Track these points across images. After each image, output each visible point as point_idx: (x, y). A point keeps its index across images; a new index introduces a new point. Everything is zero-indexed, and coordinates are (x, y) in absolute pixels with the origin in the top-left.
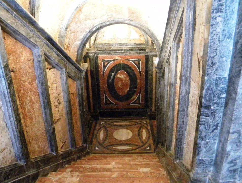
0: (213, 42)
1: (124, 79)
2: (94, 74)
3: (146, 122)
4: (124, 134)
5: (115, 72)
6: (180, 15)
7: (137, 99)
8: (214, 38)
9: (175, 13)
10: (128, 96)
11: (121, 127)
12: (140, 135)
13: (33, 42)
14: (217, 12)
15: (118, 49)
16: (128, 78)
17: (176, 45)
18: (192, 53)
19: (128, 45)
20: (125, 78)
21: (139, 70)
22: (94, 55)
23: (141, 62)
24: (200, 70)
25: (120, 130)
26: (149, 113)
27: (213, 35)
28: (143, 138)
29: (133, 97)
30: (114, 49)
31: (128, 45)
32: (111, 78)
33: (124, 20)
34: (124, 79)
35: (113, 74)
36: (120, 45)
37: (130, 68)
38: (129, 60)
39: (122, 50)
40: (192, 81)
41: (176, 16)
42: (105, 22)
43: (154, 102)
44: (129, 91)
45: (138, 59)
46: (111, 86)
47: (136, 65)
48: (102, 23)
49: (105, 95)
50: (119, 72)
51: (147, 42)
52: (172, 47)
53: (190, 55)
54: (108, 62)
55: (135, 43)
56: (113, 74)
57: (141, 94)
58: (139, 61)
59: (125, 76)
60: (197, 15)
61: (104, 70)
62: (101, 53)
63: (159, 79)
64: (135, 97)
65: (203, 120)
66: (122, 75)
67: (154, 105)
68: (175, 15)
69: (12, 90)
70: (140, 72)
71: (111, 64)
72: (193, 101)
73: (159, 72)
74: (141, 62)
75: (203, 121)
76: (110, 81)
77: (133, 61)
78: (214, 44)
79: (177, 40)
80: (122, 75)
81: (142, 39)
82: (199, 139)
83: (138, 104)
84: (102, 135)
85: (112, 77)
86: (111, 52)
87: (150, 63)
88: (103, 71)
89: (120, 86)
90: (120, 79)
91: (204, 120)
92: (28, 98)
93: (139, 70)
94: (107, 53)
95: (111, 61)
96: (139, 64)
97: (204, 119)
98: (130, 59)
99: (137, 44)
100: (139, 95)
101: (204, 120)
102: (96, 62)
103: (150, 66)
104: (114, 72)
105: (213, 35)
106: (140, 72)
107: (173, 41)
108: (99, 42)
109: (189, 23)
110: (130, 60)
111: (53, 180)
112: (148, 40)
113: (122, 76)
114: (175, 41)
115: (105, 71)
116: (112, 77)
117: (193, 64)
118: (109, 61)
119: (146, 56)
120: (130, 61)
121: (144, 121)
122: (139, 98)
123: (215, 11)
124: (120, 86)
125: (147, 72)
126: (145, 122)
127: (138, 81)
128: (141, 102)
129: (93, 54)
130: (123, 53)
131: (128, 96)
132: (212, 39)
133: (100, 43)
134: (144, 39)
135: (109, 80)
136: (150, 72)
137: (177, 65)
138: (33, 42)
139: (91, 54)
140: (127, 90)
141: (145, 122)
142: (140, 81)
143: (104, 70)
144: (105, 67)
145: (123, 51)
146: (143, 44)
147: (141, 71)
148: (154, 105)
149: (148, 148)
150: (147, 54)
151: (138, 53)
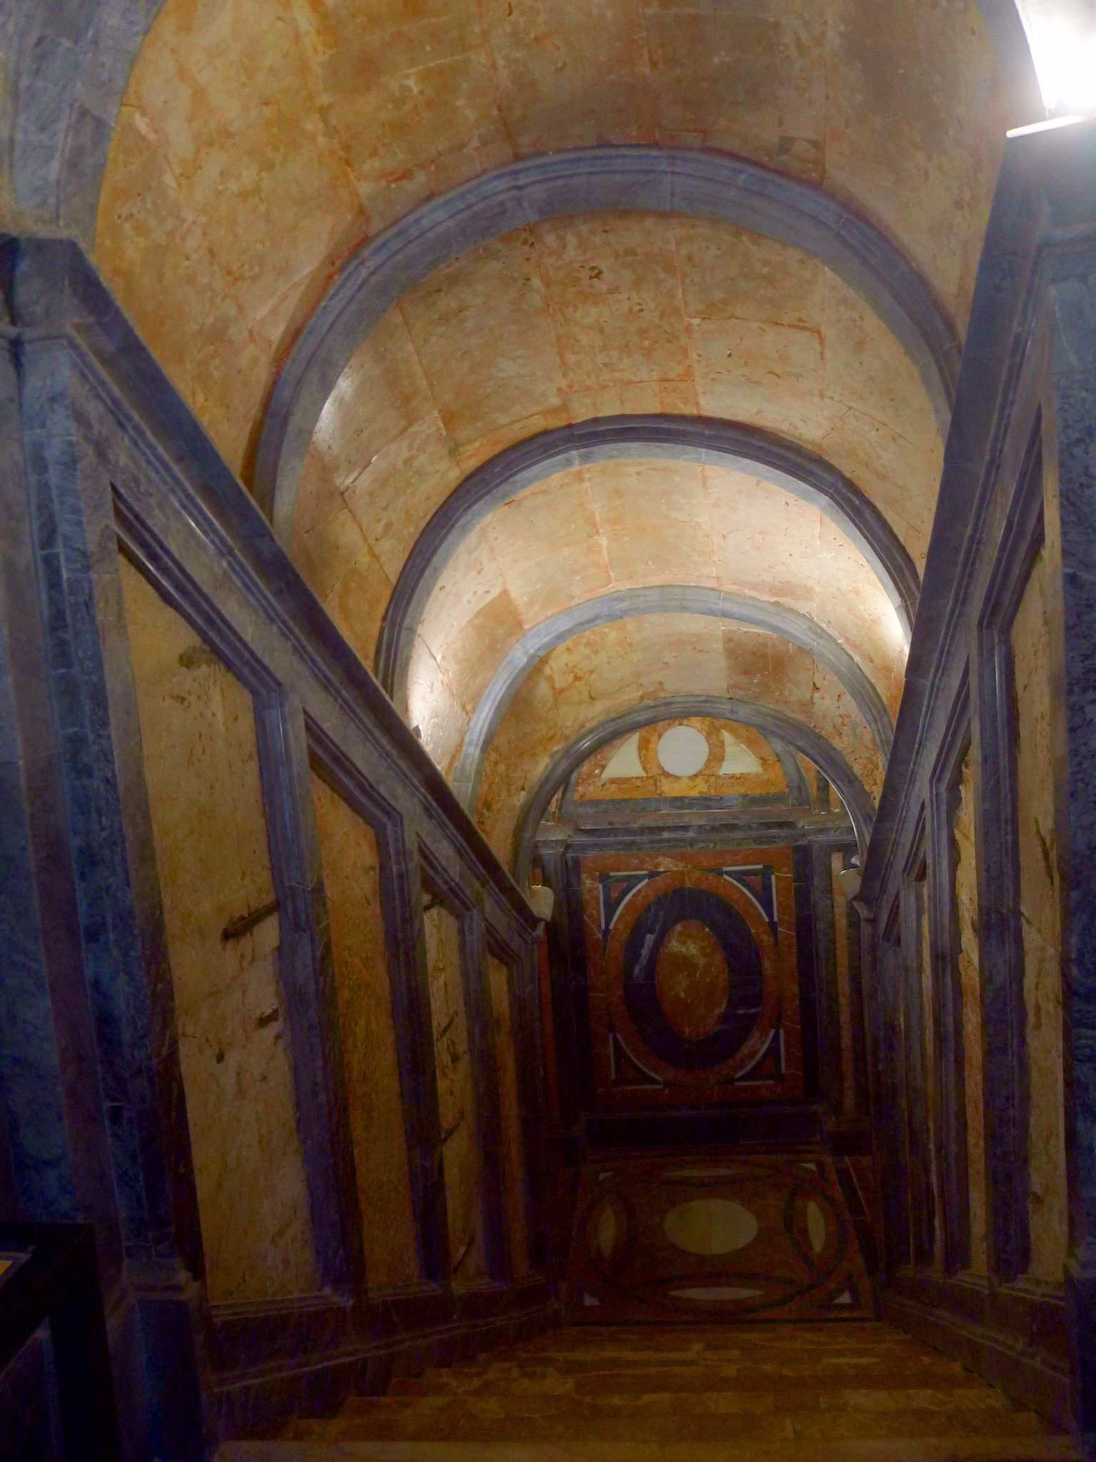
0: (1082, 780)
1: (701, 962)
2: (567, 943)
3: (820, 1164)
4: (718, 1225)
5: (658, 927)
6: (955, 683)
7: (765, 1055)
8: (1085, 766)
9: (935, 675)
10: (723, 1045)
11: (711, 1189)
12: (794, 1226)
13: (384, 799)
14: (1085, 690)
15: (670, 823)
16: (719, 958)
17: (944, 795)
18: (1014, 821)
19: (712, 804)
20: (705, 956)
21: (770, 915)
22: (564, 855)
23: (778, 879)
24: (1052, 878)
25: (697, 1205)
26: (830, 1124)
27: (1079, 759)
28: (810, 1247)
29: (745, 1050)
30: (652, 824)
31: (712, 804)
32: (640, 955)
33: (712, 702)
34: (701, 962)
35: (650, 939)
36: (678, 804)
37: (727, 910)
38: (721, 873)
39: (685, 828)
40: (1025, 927)
41: (938, 688)
42: (629, 714)
43: (848, 1066)
44: (725, 1018)
45: (760, 867)
46: (643, 999)
47: (755, 894)
48: (620, 717)
49: (616, 1040)
50: (679, 928)
51: (801, 786)
52: (927, 803)
53: (1009, 828)
54: (625, 884)
55: (745, 796)
56: (650, 939)
57: (782, 1032)
58: (766, 874)
59: (702, 949)
60: (1019, 685)
61: (607, 924)
62: (595, 845)
63: (874, 947)
64: (758, 1044)
65: (1084, 1041)
66: (690, 942)
67: (849, 1082)
68: (933, 684)
69: (328, 979)
70: (773, 925)
71: (639, 891)
72: (1041, 1002)
73: (872, 916)
74: (773, 877)
75: (1087, 1046)
76: (637, 970)
77: (740, 876)
78: (1087, 784)
79: (947, 776)
80: (688, 944)
81: (776, 773)
82: (1080, 1117)
83: (771, 1082)
84: (607, 1231)
85: (645, 952)
86: (638, 839)
87: (816, 881)
88: (603, 927)
89: (682, 994)
90: (685, 963)
91: (1090, 1042)
92: (362, 1022)
93: (770, 915)
94: (621, 843)
95: (639, 879)
96: (768, 888)
97: (1087, 1038)
98: (726, 869)
99: (754, 801)
100: (776, 1037)
101: (1090, 1042)
102: (568, 885)
103: (816, 896)
104: (651, 932)
105: (1079, 759)
106: (773, 925)
107: (931, 781)
108: (584, 794)
109: (995, 715)
110: (728, 873)
111: (459, 1391)
112: (802, 779)
113: (692, 949)
114: (939, 779)
115: (611, 927)
116: (645, 952)
117: (1024, 860)
118: (631, 881)
119: (797, 849)
120: (726, 877)
121: (811, 1161)
122: (773, 1051)
123: (1076, 689)
124: (682, 994)
125: (805, 927)
126: (812, 1166)
127: (767, 965)
128: (783, 1071)
129: (562, 850)
130: (692, 842)
131: (723, 1045)
132: (1078, 772)
133: (587, 797)
134: (785, 774)
135: (632, 968)
136: (821, 926)
137: (958, 873)
138: (387, 797)
139: (552, 848)
140: (717, 1012)
141: (812, 1166)
142: (778, 967)
143: (607, 924)
144: (611, 907)
145: (691, 834)
146: (779, 798)
147: (776, 919)
148: (849, 1082)
149: (845, 1298)
150: (800, 843)
151: (758, 840)
